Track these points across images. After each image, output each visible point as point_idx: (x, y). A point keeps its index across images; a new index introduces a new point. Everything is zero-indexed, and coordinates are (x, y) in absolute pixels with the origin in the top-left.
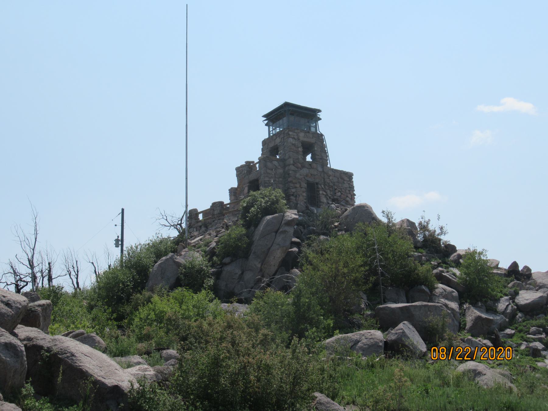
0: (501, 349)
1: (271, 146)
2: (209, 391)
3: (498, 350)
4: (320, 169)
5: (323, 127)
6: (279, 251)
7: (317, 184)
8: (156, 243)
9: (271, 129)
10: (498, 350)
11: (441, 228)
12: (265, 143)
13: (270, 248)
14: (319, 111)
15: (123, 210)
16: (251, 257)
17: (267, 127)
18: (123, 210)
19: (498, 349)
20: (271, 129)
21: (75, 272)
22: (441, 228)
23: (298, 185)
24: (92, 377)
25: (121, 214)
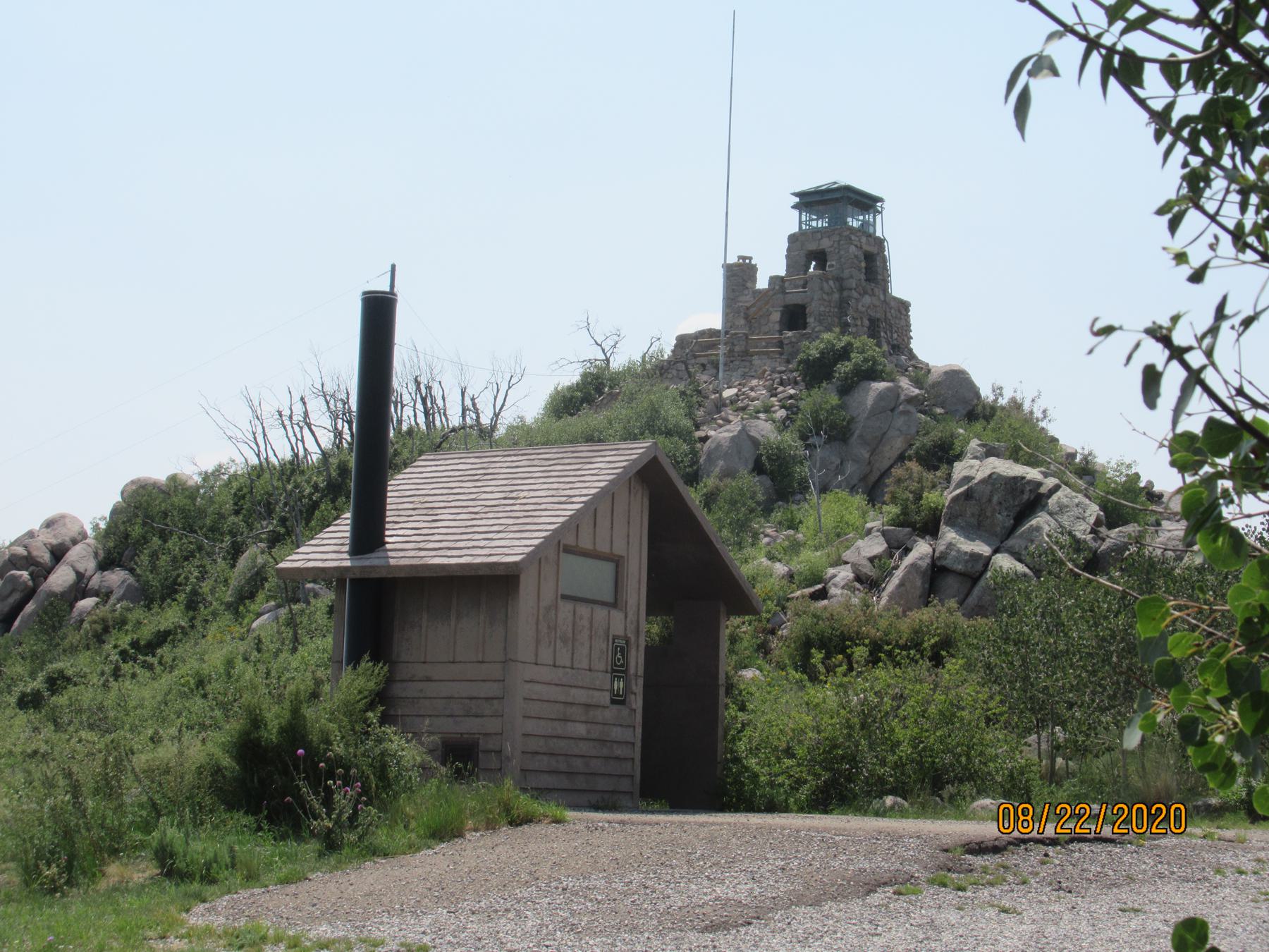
0: (1160, 809)
1: (810, 249)
2: (322, 764)
3: (1153, 812)
4: (882, 297)
5: (888, 226)
6: (900, 439)
7: (878, 320)
8: (1105, 474)
9: (803, 218)
10: (1153, 812)
11: (1044, 412)
12: (793, 239)
13: (885, 433)
14: (881, 200)
15: (393, 267)
16: (854, 440)
17: (796, 213)
18: (393, 267)
19: (1154, 808)
20: (803, 218)
21: (494, 406)
22: (1044, 412)
23: (859, 323)
24: (973, 521)
25: (389, 274)
